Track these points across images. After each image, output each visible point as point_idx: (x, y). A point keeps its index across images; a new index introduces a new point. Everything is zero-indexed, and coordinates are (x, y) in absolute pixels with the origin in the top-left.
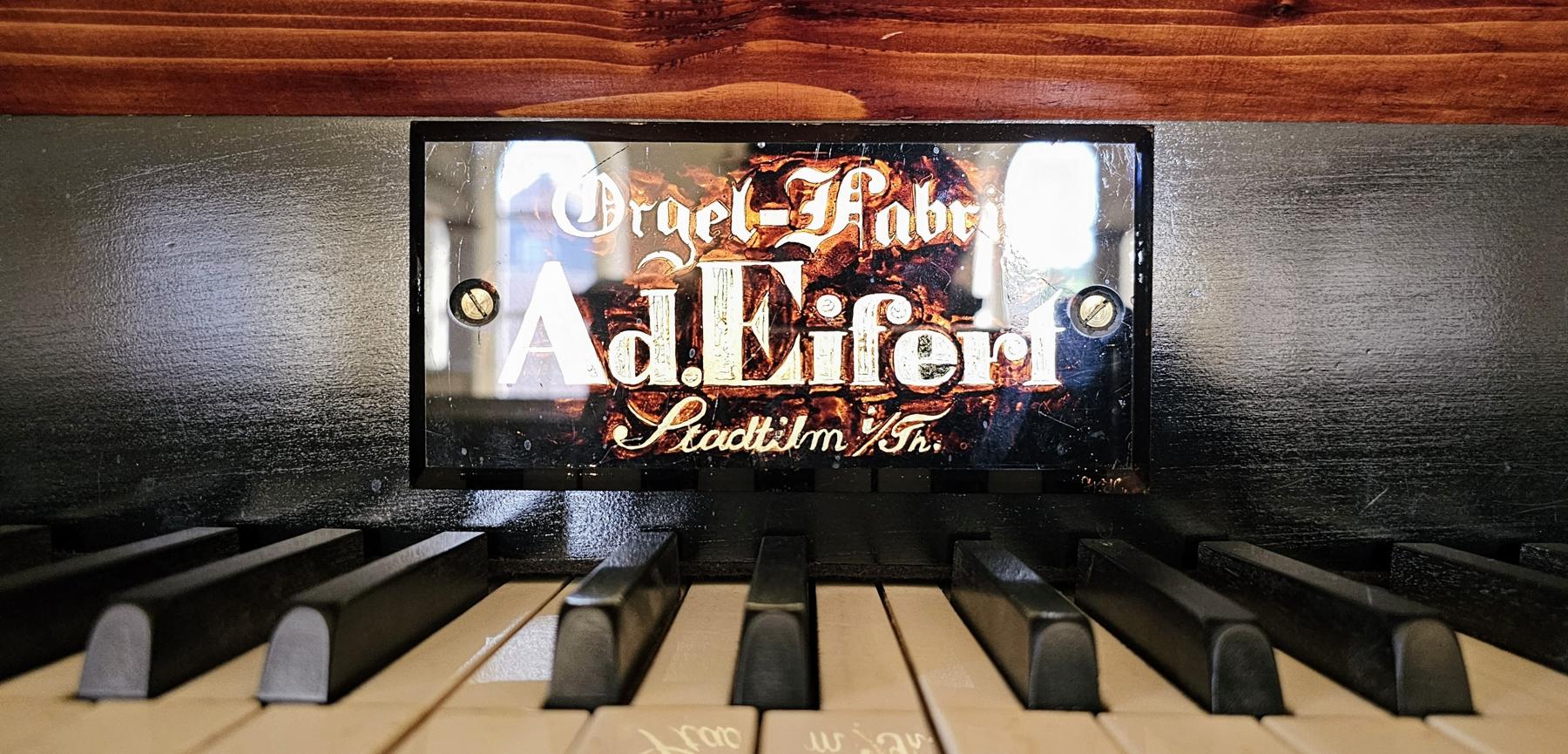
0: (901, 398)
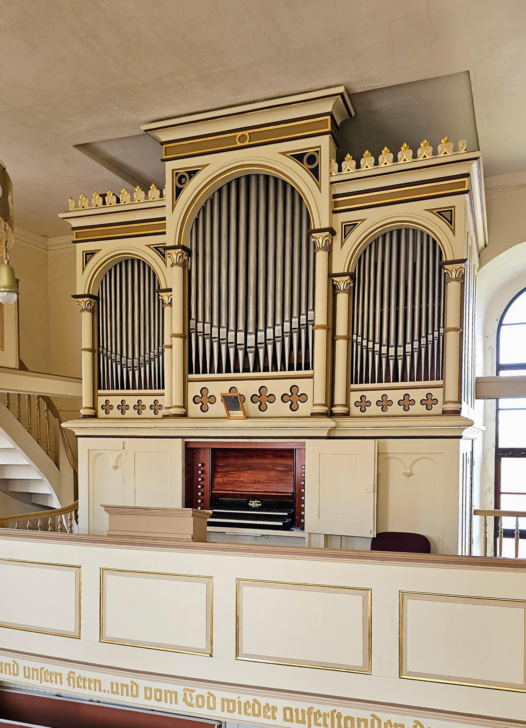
0: (257, 506)
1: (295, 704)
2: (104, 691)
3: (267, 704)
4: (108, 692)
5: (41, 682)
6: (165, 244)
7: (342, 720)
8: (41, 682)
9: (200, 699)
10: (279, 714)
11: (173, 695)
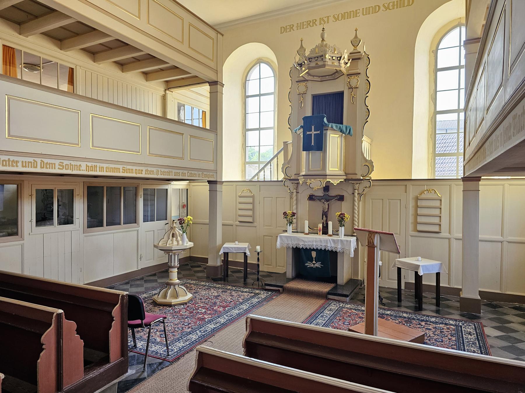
1: (163, 170)
2: (82, 170)
3: (164, 171)
4: (84, 170)
5: (157, 175)
6: (204, 113)
7: (11, 162)
8: (157, 175)
9: (4, 162)
10: (144, 172)
11: (53, 165)
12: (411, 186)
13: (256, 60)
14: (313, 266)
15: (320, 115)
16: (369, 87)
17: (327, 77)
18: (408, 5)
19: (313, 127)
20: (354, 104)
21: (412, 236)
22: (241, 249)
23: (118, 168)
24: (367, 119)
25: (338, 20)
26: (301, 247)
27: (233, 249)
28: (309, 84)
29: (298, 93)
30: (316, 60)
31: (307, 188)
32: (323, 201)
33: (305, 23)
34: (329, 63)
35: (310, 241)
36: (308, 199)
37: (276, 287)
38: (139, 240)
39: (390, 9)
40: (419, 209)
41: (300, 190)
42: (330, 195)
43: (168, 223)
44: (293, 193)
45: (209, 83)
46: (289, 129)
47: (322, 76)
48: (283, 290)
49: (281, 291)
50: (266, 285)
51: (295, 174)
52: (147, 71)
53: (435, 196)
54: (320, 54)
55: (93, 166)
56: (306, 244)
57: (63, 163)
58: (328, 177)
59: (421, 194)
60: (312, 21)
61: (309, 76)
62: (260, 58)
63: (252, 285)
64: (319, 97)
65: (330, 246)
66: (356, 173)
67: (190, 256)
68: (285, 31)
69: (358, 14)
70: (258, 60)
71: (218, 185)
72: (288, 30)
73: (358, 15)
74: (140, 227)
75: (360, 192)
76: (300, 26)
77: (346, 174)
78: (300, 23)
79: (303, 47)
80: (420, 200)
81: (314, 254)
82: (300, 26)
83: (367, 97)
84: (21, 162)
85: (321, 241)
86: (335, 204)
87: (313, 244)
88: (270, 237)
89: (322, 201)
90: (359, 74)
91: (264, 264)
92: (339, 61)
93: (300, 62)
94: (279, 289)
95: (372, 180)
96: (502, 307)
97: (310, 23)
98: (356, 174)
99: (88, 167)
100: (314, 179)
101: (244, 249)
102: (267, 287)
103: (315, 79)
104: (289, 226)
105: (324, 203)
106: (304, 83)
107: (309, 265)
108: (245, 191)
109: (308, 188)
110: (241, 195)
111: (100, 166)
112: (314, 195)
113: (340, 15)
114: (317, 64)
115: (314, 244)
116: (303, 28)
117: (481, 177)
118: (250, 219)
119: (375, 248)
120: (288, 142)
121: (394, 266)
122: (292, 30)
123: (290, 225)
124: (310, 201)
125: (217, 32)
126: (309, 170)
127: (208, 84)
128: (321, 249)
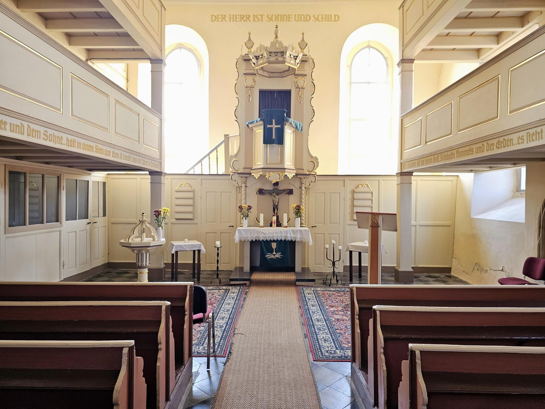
12: (348, 181)
13: (177, 44)
14: (273, 257)
15: (272, 109)
16: (314, 90)
17: (276, 74)
18: (335, 21)
19: (274, 121)
20: (301, 103)
21: (349, 225)
22: (195, 246)
23: (92, 146)
24: (312, 119)
25: (317, 21)
26: (261, 240)
27: (187, 248)
28: (257, 78)
29: (246, 86)
30: (276, 55)
31: (255, 182)
32: (275, 195)
33: (238, 16)
34: (288, 59)
35: (270, 233)
36: (256, 193)
37: (242, 281)
38: (62, 245)
39: (319, 21)
40: (355, 201)
41: (248, 184)
42: (279, 189)
43: (90, 223)
44: (241, 187)
45: (150, 61)
46: (236, 122)
47: (271, 73)
48: (251, 283)
49: (247, 284)
50: (231, 280)
51: (244, 168)
52: (73, 33)
53: (368, 190)
54: (280, 50)
55: (72, 140)
56: (266, 236)
57: (47, 132)
58: (286, 170)
59: (357, 188)
60: (245, 16)
61: (261, 70)
62: (182, 43)
63: (211, 283)
64: (263, 93)
65: (290, 237)
66: (303, 168)
67: (108, 262)
68: (216, 20)
69: (290, 19)
70: (178, 44)
71: (162, 177)
72: (220, 20)
73: (291, 20)
74: (63, 227)
75: (307, 186)
76: (233, 18)
77: (297, 169)
78: (325, 15)
79: (251, 40)
80: (356, 194)
81: (274, 245)
82: (233, 18)
83: (312, 98)
84: (9, 123)
85: (281, 232)
86: (283, 198)
87: (274, 236)
88: (214, 234)
89: (274, 195)
90: (306, 75)
91: (207, 263)
92: (295, 60)
93: (257, 55)
94: (246, 282)
95: (317, 175)
96: (420, 277)
97: (243, 17)
98: (303, 169)
99: (68, 141)
100: (273, 172)
101: (199, 246)
102: (232, 283)
103: (265, 74)
104: (245, 220)
105: (275, 196)
106: (252, 77)
107: (269, 256)
108: (184, 185)
109: (256, 182)
110: (178, 189)
111: (78, 141)
112: (263, 189)
113: (274, 17)
114: (277, 59)
115: (275, 235)
116: (236, 21)
117: (413, 173)
118: (190, 216)
119: (379, 227)
120: (229, 135)
121: (347, 250)
122: (224, 20)
123: (246, 219)
124: (259, 196)
125: (161, 5)
126: (267, 163)
127: (149, 61)
128: (281, 240)
